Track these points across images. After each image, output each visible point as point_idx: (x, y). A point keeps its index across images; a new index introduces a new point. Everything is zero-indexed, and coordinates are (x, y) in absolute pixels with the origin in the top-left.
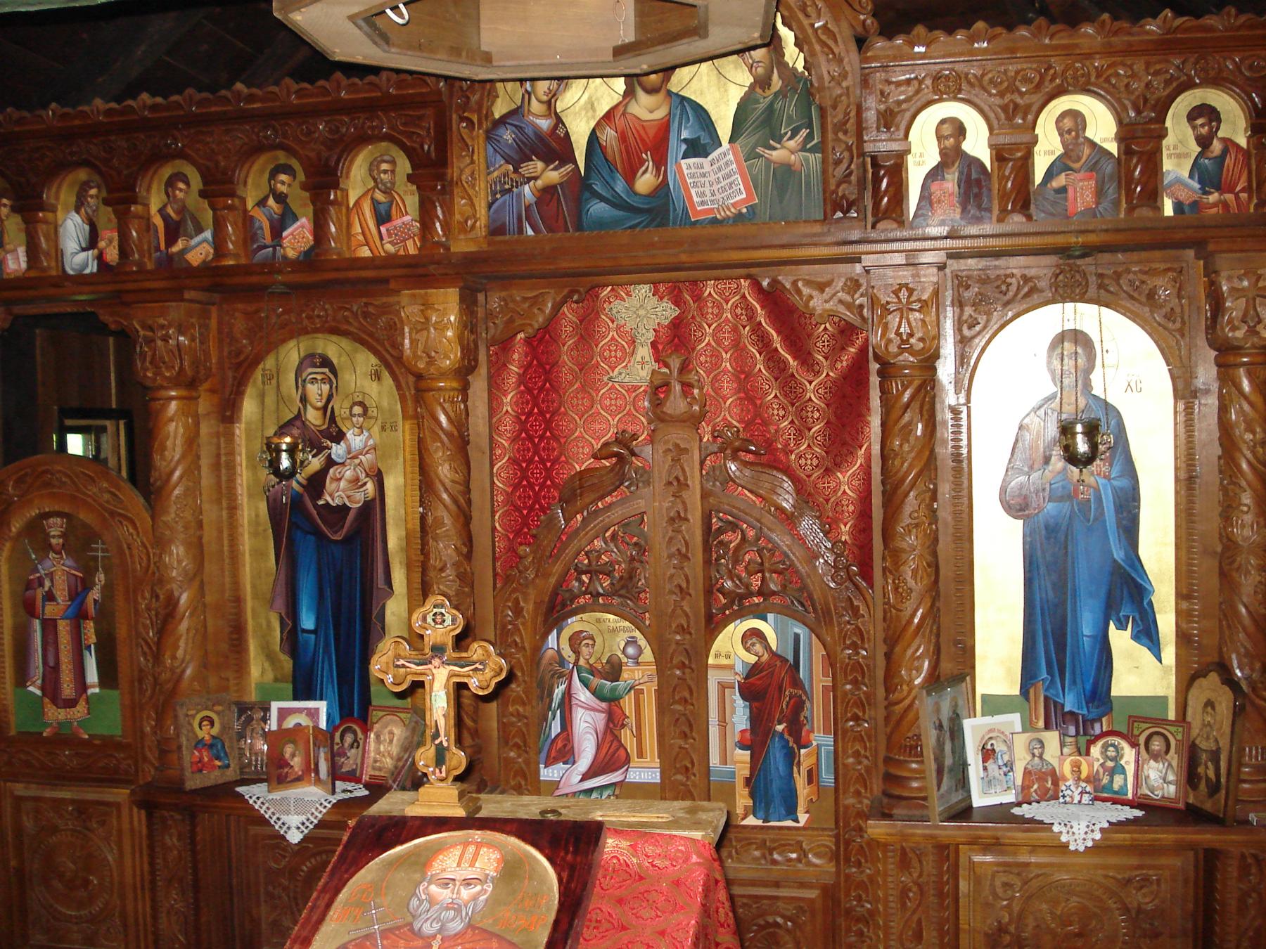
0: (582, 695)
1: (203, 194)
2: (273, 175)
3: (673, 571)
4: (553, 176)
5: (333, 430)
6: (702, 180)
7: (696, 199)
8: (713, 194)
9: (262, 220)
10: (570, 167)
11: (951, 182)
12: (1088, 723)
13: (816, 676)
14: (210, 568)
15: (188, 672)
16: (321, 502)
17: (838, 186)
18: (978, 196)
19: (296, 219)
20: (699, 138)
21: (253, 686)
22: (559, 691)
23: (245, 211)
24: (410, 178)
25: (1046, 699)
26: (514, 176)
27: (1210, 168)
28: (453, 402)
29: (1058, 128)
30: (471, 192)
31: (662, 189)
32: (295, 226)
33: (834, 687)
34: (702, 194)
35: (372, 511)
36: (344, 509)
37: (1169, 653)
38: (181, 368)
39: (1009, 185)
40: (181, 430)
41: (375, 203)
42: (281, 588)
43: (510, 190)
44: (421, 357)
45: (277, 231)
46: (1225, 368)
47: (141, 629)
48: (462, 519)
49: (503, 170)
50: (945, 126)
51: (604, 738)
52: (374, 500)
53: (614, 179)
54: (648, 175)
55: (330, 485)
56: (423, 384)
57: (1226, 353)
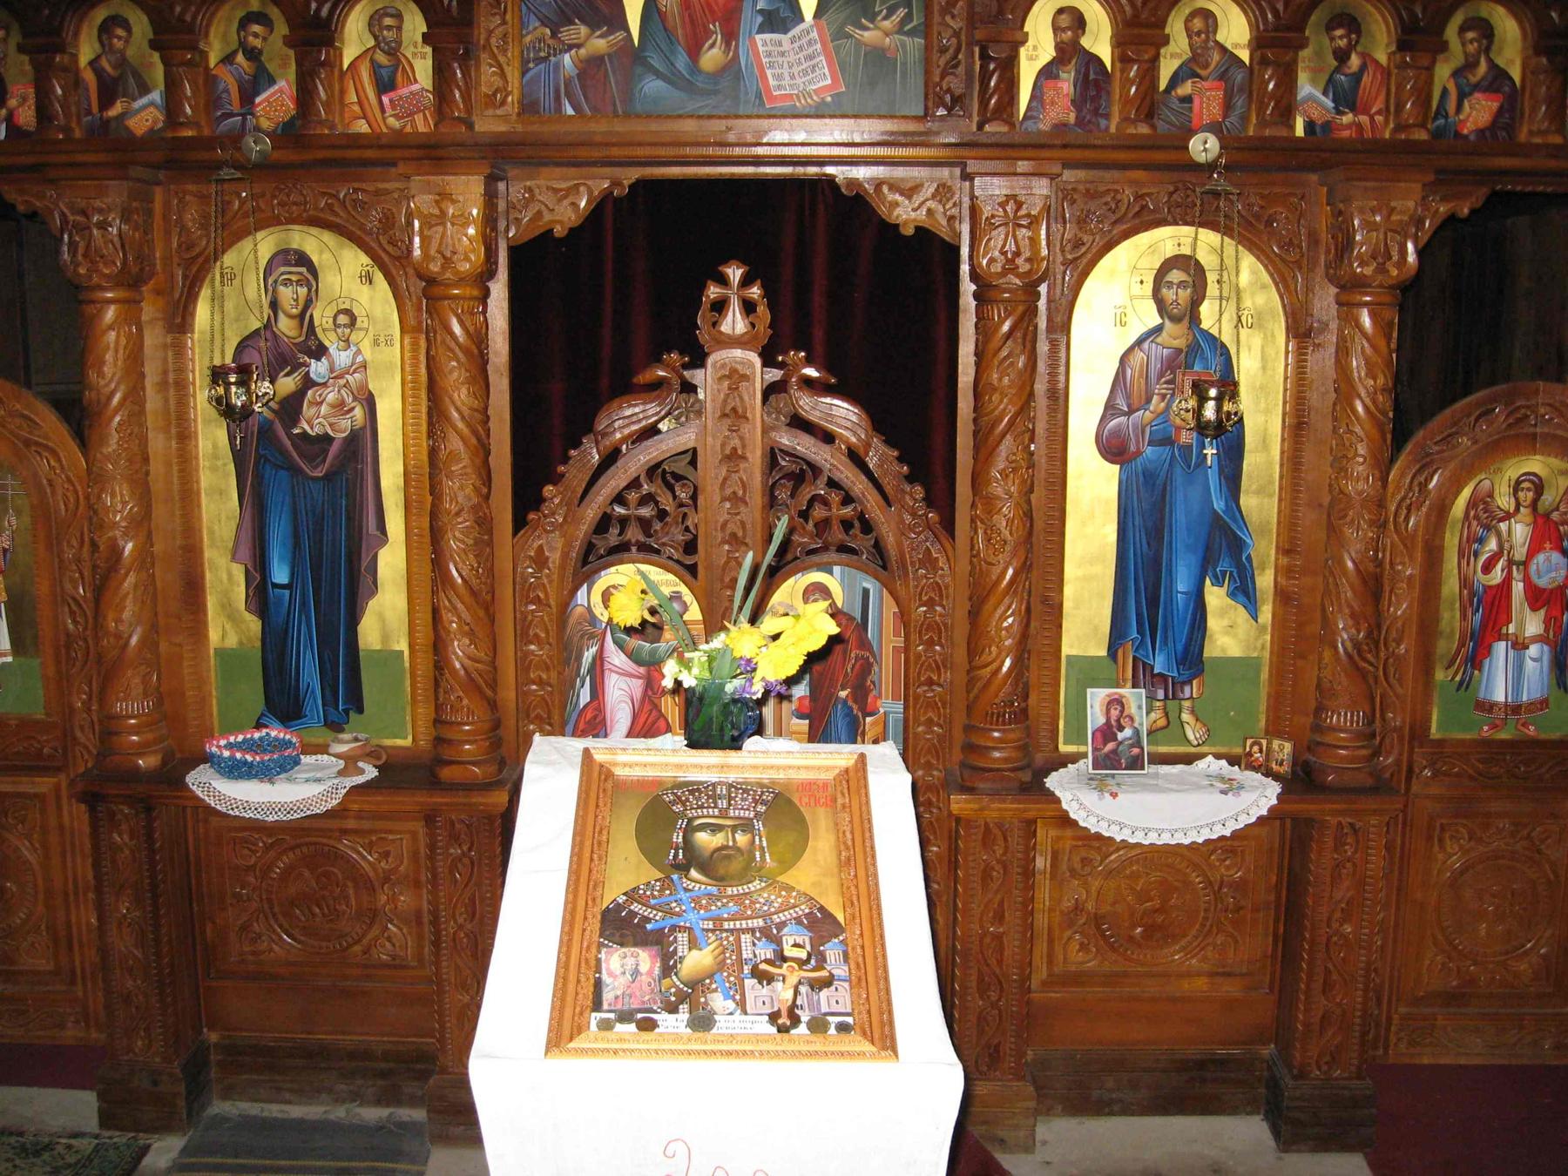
0: (616, 658)
1: (154, 45)
2: (244, 23)
3: (726, 516)
4: (599, 44)
5: (312, 344)
6: (780, 60)
7: (772, 82)
8: (792, 77)
9: (228, 81)
10: (620, 35)
11: (1067, 83)
12: (1179, 685)
13: (885, 635)
14: (159, 511)
15: (134, 640)
16: (296, 431)
17: (942, 78)
18: (1094, 99)
19: (272, 81)
20: (778, 9)
21: (212, 652)
22: (588, 655)
23: (207, 68)
24: (426, 38)
25: (1135, 658)
26: (551, 42)
27: (1346, 86)
28: (472, 314)
29: (1187, 29)
30: (502, 59)
31: (731, 69)
32: (272, 90)
33: (906, 649)
34: (779, 77)
35: (361, 445)
36: (326, 439)
37: (1266, 613)
38: (125, 263)
39: (1133, 90)
40: (123, 341)
41: (375, 67)
42: (247, 536)
43: (545, 59)
44: (434, 259)
45: (248, 95)
46: (1347, 308)
47: (68, 586)
48: (482, 454)
49: (538, 33)
50: (1063, 16)
51: (641, 709)
52: (363, 428)
53: (673, 52)
54: (715, 51)
55: (307, 411)
56: (437, 291)
57: (1349, 287)
